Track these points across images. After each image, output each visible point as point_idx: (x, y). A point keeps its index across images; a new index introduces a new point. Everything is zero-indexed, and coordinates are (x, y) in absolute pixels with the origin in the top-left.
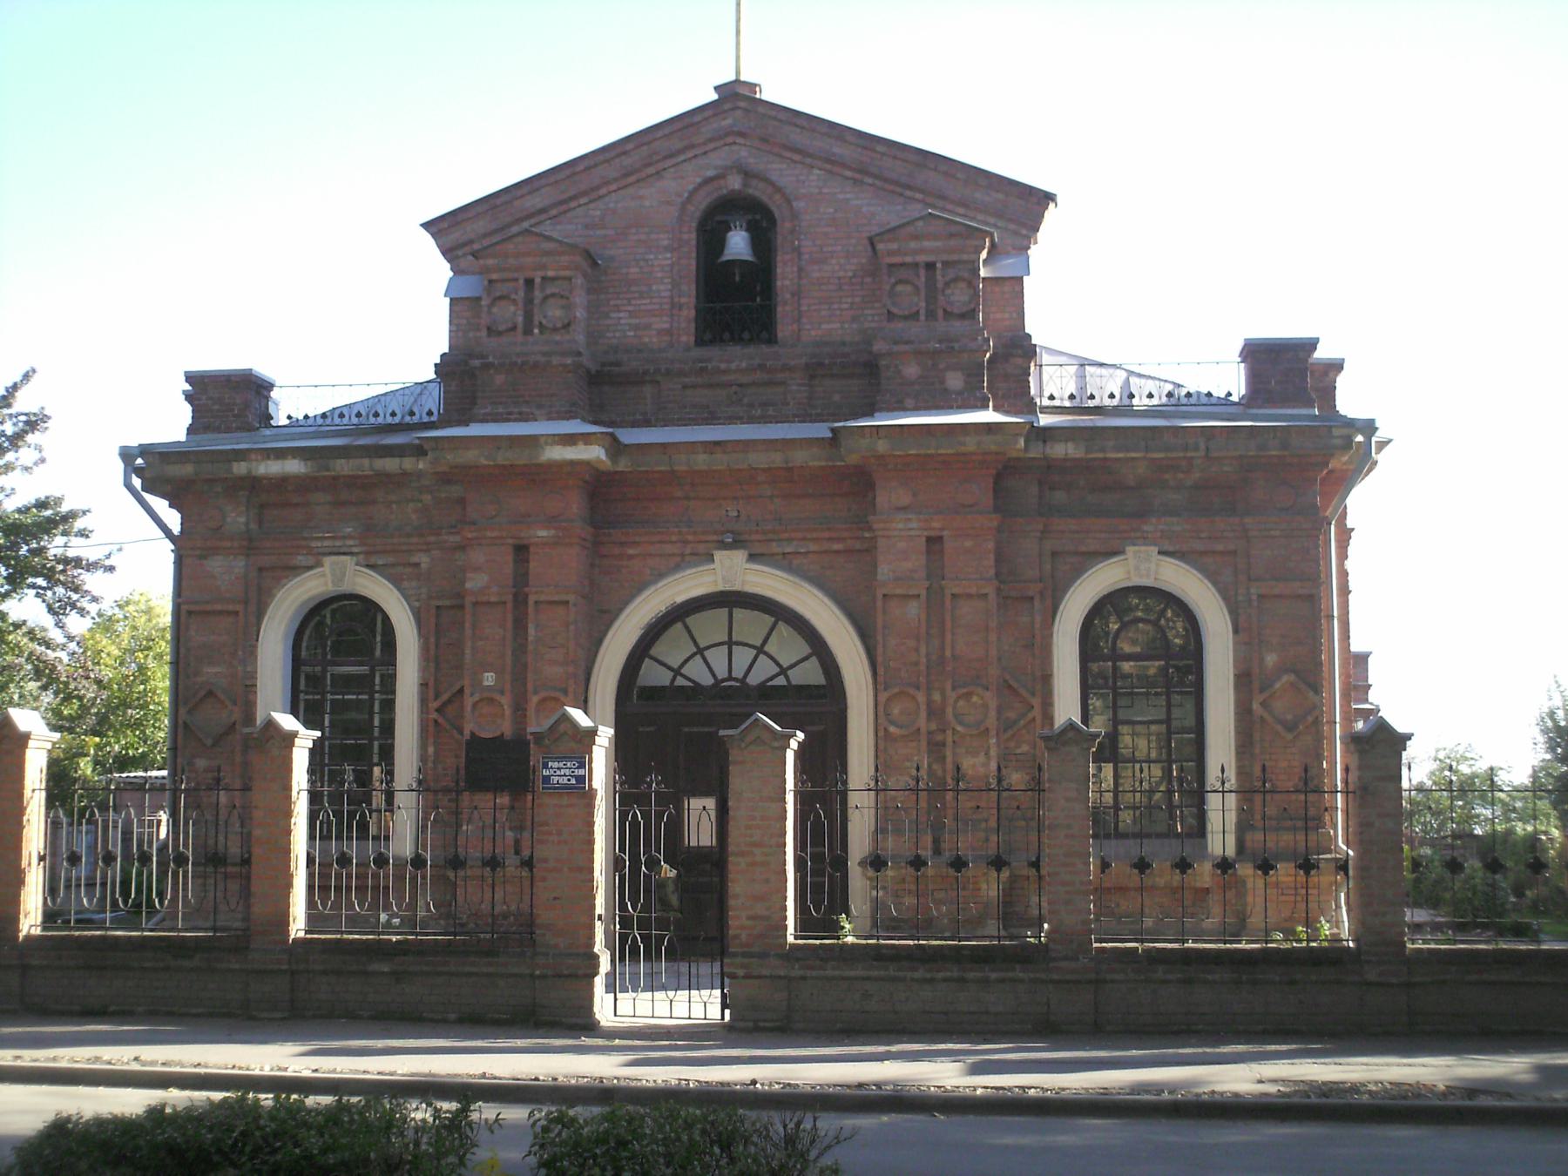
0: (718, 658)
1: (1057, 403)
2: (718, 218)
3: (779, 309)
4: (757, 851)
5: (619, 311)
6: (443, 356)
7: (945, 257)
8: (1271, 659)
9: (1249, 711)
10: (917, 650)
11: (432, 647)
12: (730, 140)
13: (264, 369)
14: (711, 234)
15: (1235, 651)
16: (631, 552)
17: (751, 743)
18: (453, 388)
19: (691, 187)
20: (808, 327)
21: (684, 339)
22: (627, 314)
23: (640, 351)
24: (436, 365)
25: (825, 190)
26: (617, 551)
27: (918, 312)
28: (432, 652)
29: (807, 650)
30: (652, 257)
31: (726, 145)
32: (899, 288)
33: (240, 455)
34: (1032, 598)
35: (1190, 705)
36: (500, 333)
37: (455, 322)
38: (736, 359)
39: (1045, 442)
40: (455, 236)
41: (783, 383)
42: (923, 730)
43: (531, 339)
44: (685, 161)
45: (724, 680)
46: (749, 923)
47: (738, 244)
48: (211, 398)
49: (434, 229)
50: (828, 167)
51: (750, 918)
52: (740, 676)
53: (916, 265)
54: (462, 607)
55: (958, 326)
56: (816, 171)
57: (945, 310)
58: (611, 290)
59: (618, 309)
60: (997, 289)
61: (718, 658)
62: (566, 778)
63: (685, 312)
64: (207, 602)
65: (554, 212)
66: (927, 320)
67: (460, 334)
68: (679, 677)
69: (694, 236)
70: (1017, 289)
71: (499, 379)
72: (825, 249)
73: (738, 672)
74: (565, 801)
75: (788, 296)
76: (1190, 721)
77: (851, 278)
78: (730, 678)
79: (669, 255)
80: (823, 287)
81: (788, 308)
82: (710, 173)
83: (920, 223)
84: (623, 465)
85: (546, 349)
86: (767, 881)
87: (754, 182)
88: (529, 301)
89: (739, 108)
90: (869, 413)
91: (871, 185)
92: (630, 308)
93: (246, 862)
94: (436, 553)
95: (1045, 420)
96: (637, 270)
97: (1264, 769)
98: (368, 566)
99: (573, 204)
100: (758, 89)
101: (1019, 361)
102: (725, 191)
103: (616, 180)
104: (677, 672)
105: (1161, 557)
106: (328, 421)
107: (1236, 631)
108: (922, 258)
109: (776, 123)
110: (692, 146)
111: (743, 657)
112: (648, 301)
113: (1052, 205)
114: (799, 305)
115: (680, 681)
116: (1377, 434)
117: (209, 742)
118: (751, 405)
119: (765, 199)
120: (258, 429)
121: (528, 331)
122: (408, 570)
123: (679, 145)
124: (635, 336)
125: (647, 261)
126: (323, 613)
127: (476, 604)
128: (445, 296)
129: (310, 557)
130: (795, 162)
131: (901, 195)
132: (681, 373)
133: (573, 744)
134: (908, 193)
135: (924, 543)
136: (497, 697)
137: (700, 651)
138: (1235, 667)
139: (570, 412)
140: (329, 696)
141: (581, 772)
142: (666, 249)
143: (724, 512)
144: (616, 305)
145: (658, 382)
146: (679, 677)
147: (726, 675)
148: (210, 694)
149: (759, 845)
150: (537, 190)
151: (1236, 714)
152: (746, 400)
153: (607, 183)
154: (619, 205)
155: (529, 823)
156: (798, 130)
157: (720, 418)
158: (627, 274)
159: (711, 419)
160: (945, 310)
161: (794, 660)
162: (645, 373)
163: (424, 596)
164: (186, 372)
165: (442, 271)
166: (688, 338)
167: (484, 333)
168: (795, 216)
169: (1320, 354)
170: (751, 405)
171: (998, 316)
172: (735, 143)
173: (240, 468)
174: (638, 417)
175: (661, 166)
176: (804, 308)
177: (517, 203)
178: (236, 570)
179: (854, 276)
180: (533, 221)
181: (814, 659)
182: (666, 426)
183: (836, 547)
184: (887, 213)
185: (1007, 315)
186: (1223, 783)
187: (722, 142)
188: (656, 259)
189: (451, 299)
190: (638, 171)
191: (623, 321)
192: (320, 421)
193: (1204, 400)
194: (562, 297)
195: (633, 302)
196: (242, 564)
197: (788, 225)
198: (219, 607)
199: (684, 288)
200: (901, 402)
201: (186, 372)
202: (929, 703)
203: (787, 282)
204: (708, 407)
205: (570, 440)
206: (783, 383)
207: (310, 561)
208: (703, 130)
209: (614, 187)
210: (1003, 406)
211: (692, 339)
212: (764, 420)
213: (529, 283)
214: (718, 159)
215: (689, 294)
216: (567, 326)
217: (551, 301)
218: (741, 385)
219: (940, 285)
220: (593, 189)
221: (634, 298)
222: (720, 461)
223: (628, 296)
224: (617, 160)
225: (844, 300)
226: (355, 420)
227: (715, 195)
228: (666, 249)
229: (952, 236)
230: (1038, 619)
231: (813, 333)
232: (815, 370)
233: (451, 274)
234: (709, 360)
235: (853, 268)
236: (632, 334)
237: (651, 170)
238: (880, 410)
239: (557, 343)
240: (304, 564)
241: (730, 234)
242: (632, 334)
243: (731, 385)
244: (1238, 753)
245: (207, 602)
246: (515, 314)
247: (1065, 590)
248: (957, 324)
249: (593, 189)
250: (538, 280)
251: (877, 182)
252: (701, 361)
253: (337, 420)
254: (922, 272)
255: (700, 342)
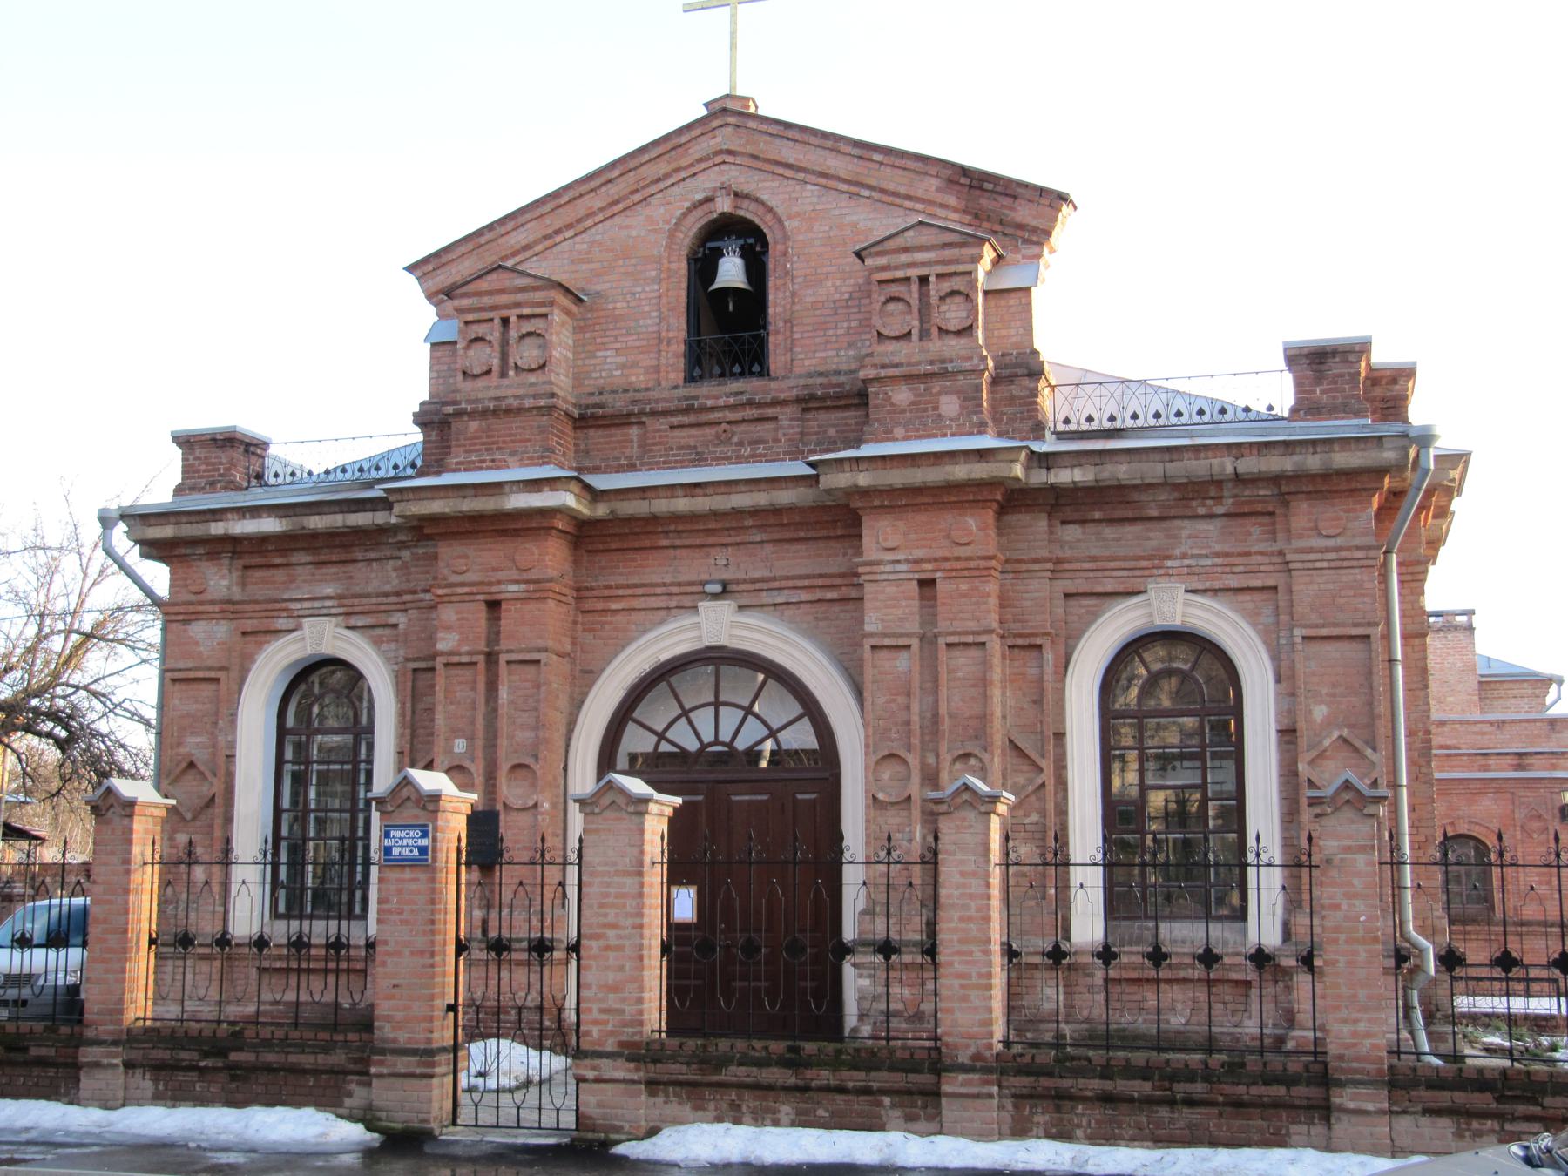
0: (704, 719)
1: (1073, 427)
2: (710, 245)
3: (771, 339)
4: (611, 933)
5: (606, 350)
6: (422, 404)
7: (940, 269)
8: (1320, 712)
9: (1296, 774)
10: (908, 708)
11: (409, 713)
12: (718, 159)
13: (251, 424)
14: (703, 265)
15: (1277, 702)
16: (614, 606)
17: (606, 808)
18: (433, 438)
19: (678, 213)
20: (800, 356)
21: (672, 376)
22: (614, 353)
23: (626, 391)
24: (414, 414)
25: (818, 207)
26: (599, 605)
27: (910, 332)
28: (408, 718)
29: (797, 709)
30: (639, 289)
31: (715, 165)
32: (891, 307)
33: (216, 514)
34: (1040, 647)
35: (1230, 765)
36: (476, 376)
37: (435, 368)
38: (717, 392)
39: (1048, 469)
40: (444, 279)
41: (775, 419)
42: (916, 797)
43: (506, 382)
44: (673, 185)
45: (710, 744)
46: (604, 1017)
47: (731, 271)
48: (199, 458)
49: (419, 273)
50: (823, 181)
51: (602, 1011)
52: (727, 739)
53: (908, 279)
54: (433, 669)
55: (954, 346)
56: (809, 187)
57: (940, 328)
58: (597, 327)
59: (604, 346)
60: (1003, 303)
61: (704, 719)
62: (408, 850)
63: (674, 347)
64: (190, 670)
65: (539, 248)
66: (921, 340)
67: (441, 381)
68: (663, 742)
69: (684, 265)
70: (1023, 301)
71: (474, 425)
72: (819, 271)
73: (725, 736)
74: (408, 874)
75: (781, 324)
76: (1230, 787)
77: (847, 301)
78: (716, 742)
79: (656, 287)
80: (818, 313)
81: (780, 337)
82: (699, 197)
83: (911, 233)
84: (602, 510)
85: (521, 392)
86: (621, 968)
87: (746, 203)
88: (505, 343)
89: (727, 124)
90: (857, 443)
91: (868, 198)
92: (619, 345)
93: (931, 951)
94: (413, 613)
95: (1047, 445)
96: (625, 305)
97: (1310, 839)
98: (348, 628)
99: (559, 238)
100: (751, 103)
101: (1026, 382)
102: (715, 215)
103: (602, 209)
104: (661, 736)
105: (1191, 596)
106: (331, 477)
107: (1278, 680)
108: (914, 273)
109: (768, 138)
110: (677, 170)
111: (730, 718)
112: (635, 337)
113: (1065, 209)
114: (792, 332)
115: (665, 747)
116: (1438, 444)
117: (189, 816)
118: (740, 443)
119: (757, 221)
120: (247, 488)
121: (503, 374)
122: (387, 631)
123: (669, 168)
124: (622, 375)
125: (634, 294)
126: (311, 679)
127: (447, 665)
128: (425, 340)
129: (291, 620)
130: (788, 178)
131: (901, 206)
132: (665, 413)
133: (417, 811)
134: (907, 204)
135: (917, 588)
136: (467, 764)
137: (685, 713)
138: (1277, 721)
139: (542, 457)
140: (315, 766)
141: (387, 843)
142: (653, 280)
143: (713, 562)
144: (604, 344)
145: (644, 423)
146: (663, 742)
147: (712, 739)
148: (191, 765)
149: (614, 926)
150: (522, 225)
151: (1281, 776)
152: (735, 439)
153: (592, 214)
154: (605, 237)
155: (497, 903)
156: (791, 143)
157: (706, 459)
158: (615, 309)
159: (698, 460)
160: (940, 328)
161: (785, 721)
162: (629, 415)
163: (401, 659)
164: (1285, 343)
165: (425, 315)
166: (677, 376)
167: (460, 377)
168: (786, 237)
169: (1382, 356)
170: (740, 443)
171: (1004, 332)
172: (724, 162)
173: (217, 529)
174: (623, 461)
175: (645, 193)
176: (797, 336)
177: (501, 241)
178: (219, 635)
179: (851, 298)
180: (517, 259)
181: (806, 719)
182: (652, 469)
183: (830, 595)
184: (876, 223)
185: (1013, 332)
186: (889, 853)
187: (710, 163)
188: (644, 291)
189: (433, 345)
190: (625, 198)
191: (609, 360)
192: (323, 477)
193: (1241, 416)
194: (539, 335)
195: (620, 339)
196: (224, 629)
197: (780, 247)
198: (200, 674)
199: (673, 321)
200: (891, 432)
201: (1285, 343)
202: (924, 766)
203: (779, 309)
204: (695, 447)
205: (535, 485)
206: (775, 419)
207: (290, 624)
208: (691, 151)
209: (600, 217)
210: (1008, 432)
211: (682, 375)
212: (754, 458)
213: (505, 322)
214: (706, 182)
215: (677, 327)
216: (542, 367)
217: (528, 341)
218: (729, 423)
219: (934, 300)
220: (579, 221)
221: (622, 335)
222: (702, 503)
223: (616, 332)
224: (603, 189)
225: (839, 325)
226: (357, 474)
227: (706, 220)
228: (653, 280)
229: (945, 245)
230: (1049, 669)
231: (807, 363)
232: (808, 402)
233: (436, 318)
234: (696, 398)
235: (850, 289)
236: (619, 373)
237: (637, 197)
238: (867, 441)
239: (532, 385)
240: (284, 628)
241: (722, 261)
242: (619, 373)
243: (720, 423)
244: (1283, 822)
245: (190, 670)
246: (490, 355)
247: (1078, 638)
248: (953, 342)
249: (579, 221)
250: (513, 319)
251: (873, 194)
252: (687, 398)
253: (340, 476)
254: (915, 287)
255: (690, 379)
